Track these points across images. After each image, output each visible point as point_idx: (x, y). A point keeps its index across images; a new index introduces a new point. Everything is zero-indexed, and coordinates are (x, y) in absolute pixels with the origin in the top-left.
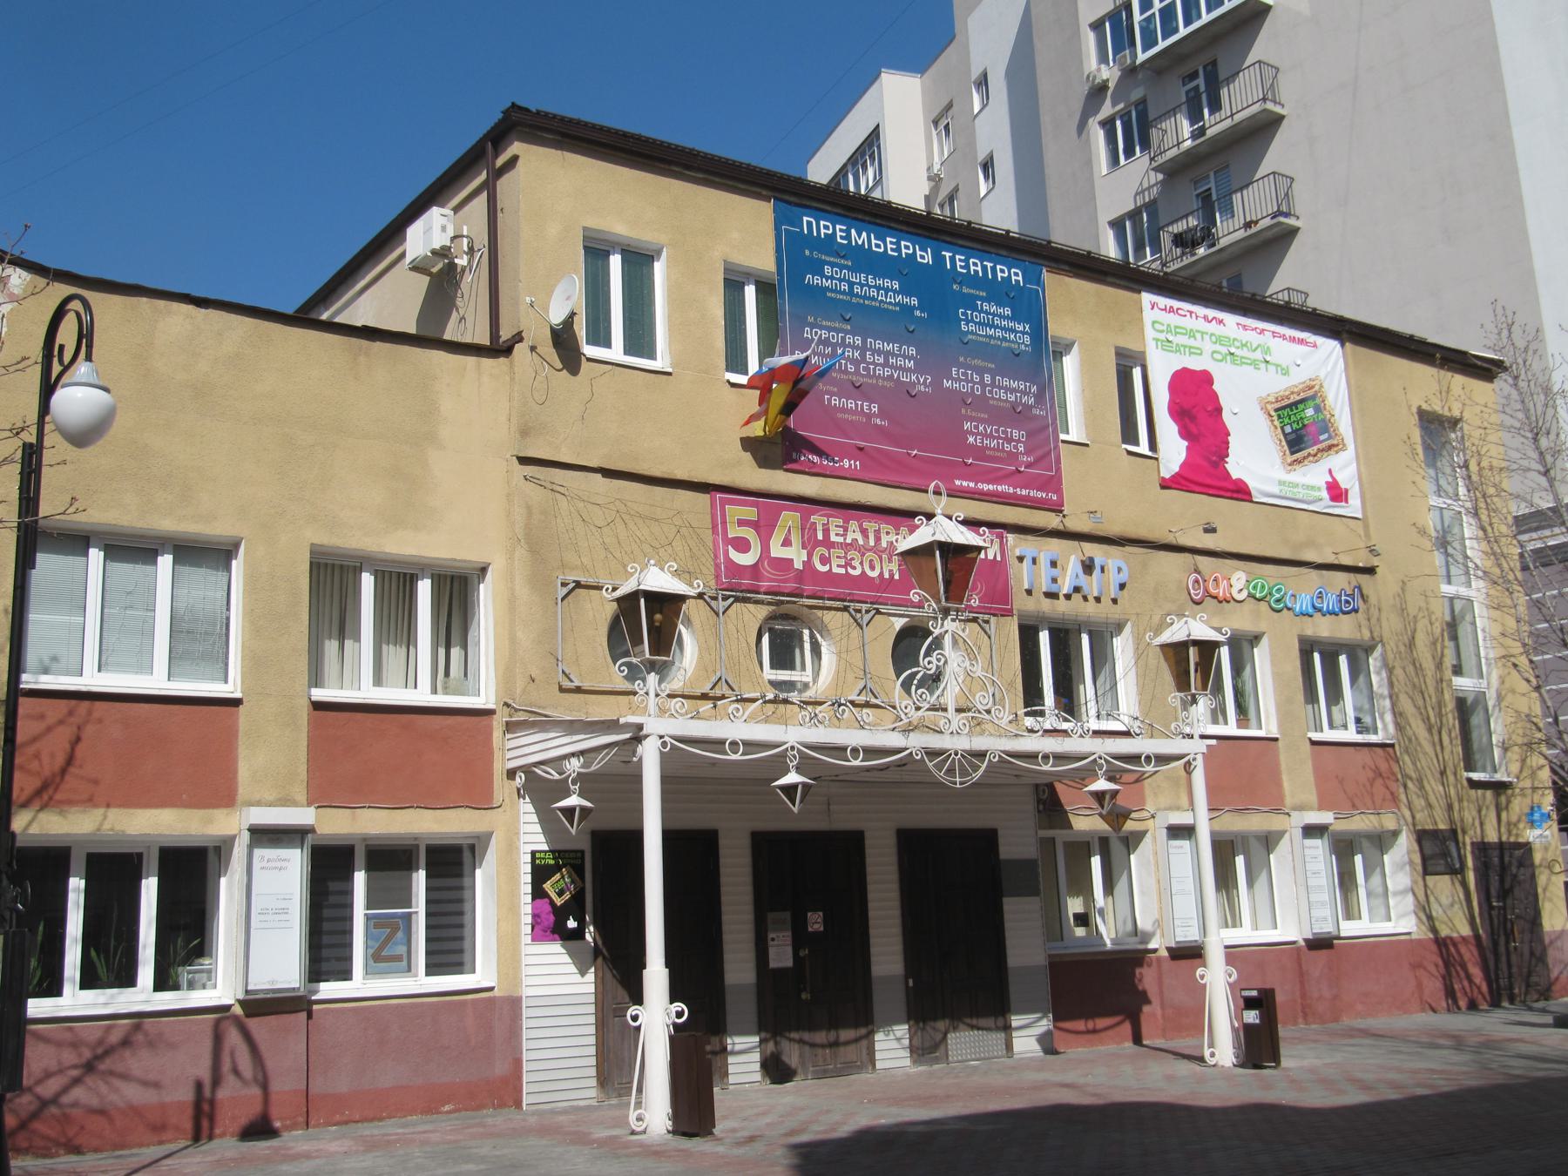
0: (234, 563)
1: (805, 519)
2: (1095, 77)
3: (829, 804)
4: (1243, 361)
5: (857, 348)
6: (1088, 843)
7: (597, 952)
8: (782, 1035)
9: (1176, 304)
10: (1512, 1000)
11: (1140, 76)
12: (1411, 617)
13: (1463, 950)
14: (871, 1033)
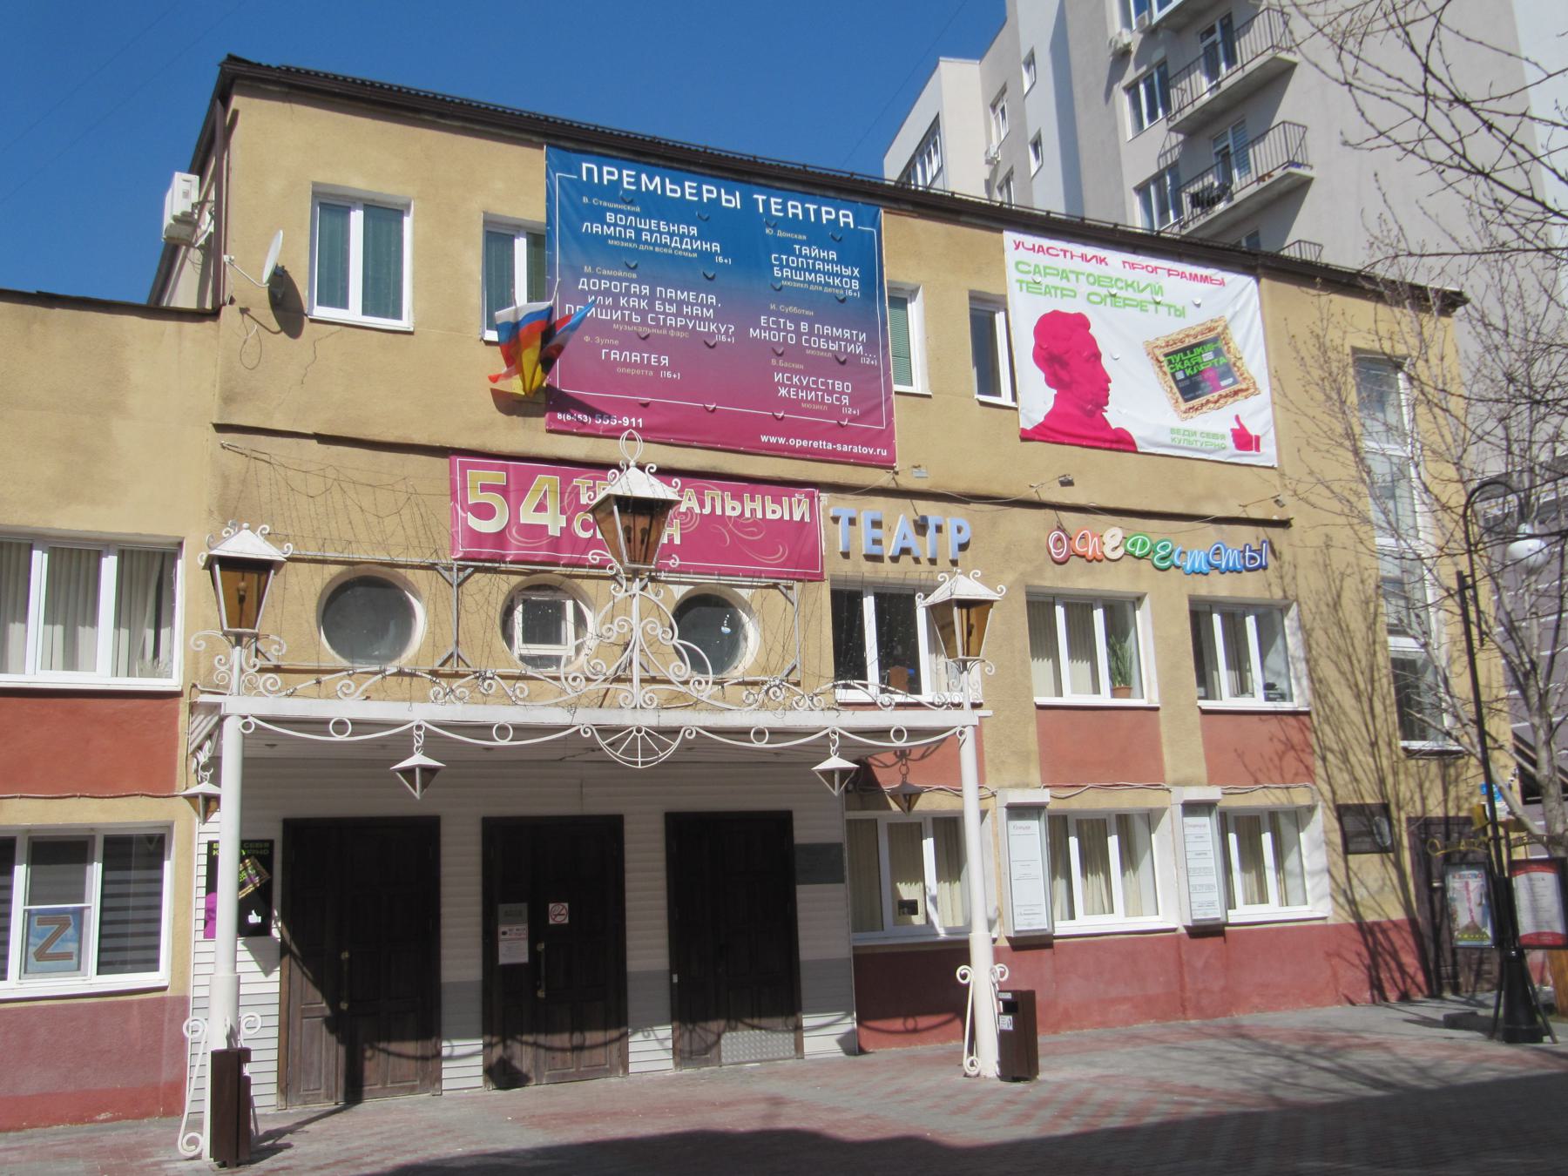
0: (179, 562)
1: (566, 482)
2: (1116, 42)
3: (581, 786)
4: (1126, 303)
5: (644, 297)
6: (920, 824)
7: (284, 949)
8: (513, 1038)
9: (1046, 243)
10: (1456, 990)
11: (1161, 36)
12: (1337, 573)
13: (1393, 935)
14: (625, 1035)
